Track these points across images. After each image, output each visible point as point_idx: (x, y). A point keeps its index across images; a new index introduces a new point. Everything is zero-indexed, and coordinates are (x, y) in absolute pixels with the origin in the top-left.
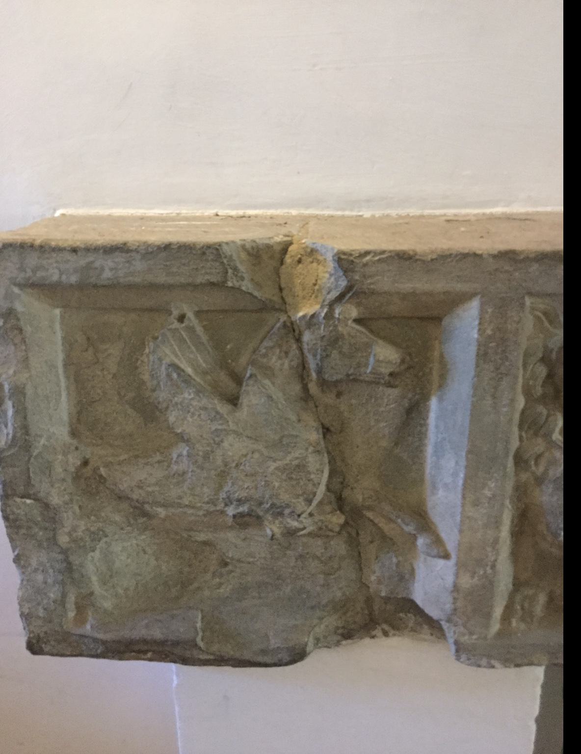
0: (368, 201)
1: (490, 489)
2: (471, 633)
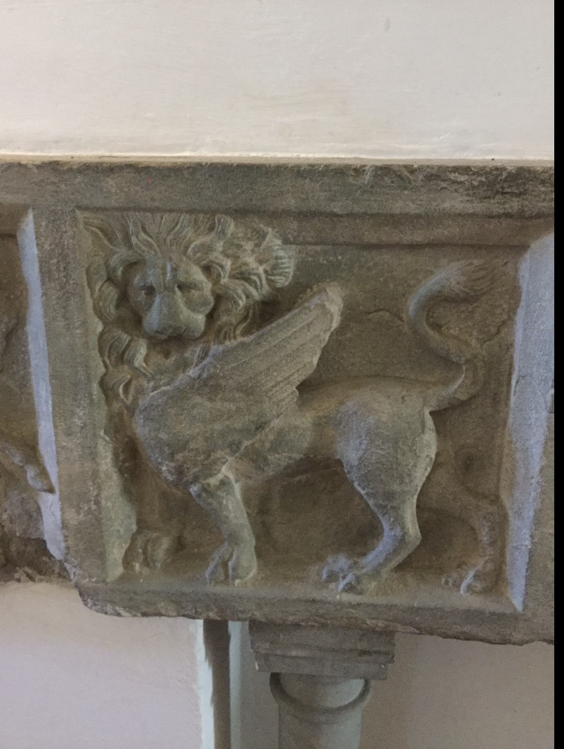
0: (57, 142)
1: (80, 418)
2: (90, 577)
